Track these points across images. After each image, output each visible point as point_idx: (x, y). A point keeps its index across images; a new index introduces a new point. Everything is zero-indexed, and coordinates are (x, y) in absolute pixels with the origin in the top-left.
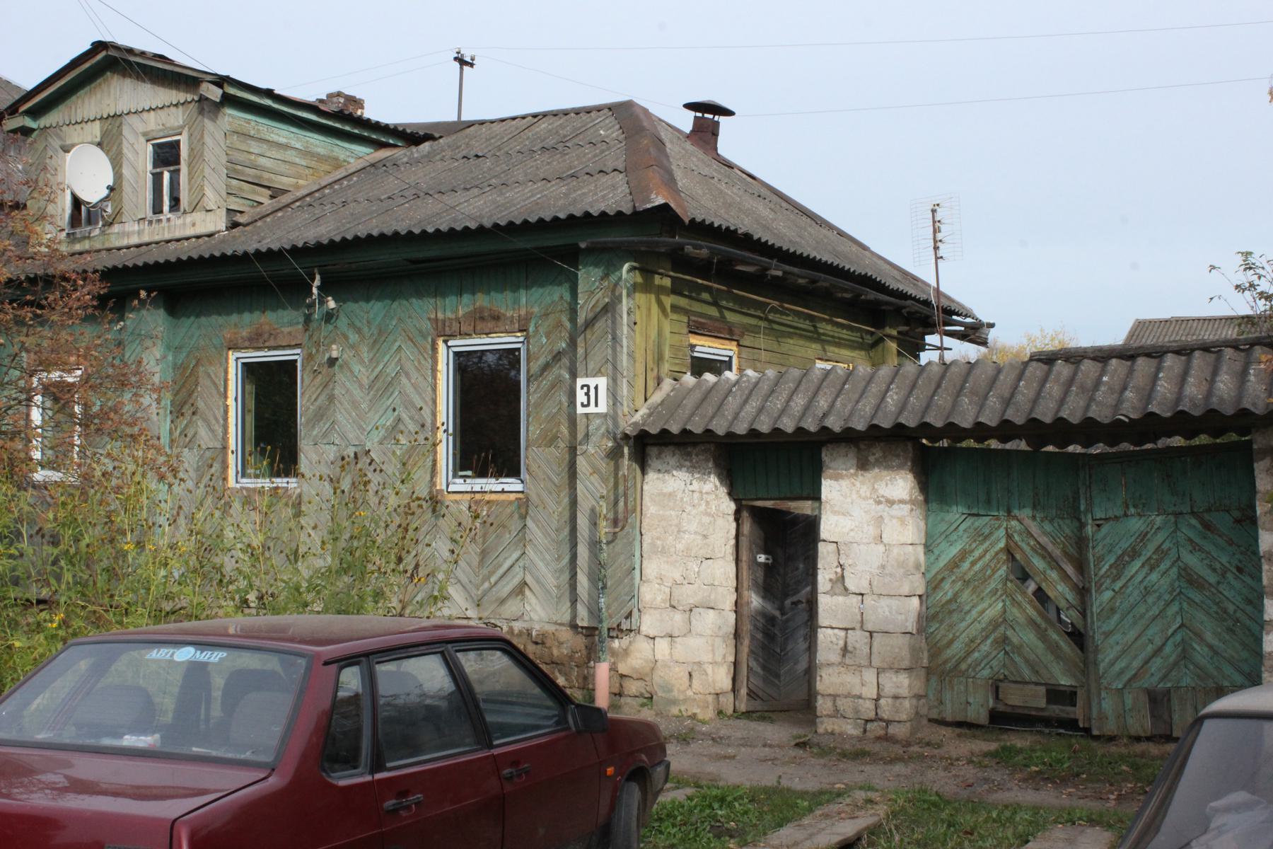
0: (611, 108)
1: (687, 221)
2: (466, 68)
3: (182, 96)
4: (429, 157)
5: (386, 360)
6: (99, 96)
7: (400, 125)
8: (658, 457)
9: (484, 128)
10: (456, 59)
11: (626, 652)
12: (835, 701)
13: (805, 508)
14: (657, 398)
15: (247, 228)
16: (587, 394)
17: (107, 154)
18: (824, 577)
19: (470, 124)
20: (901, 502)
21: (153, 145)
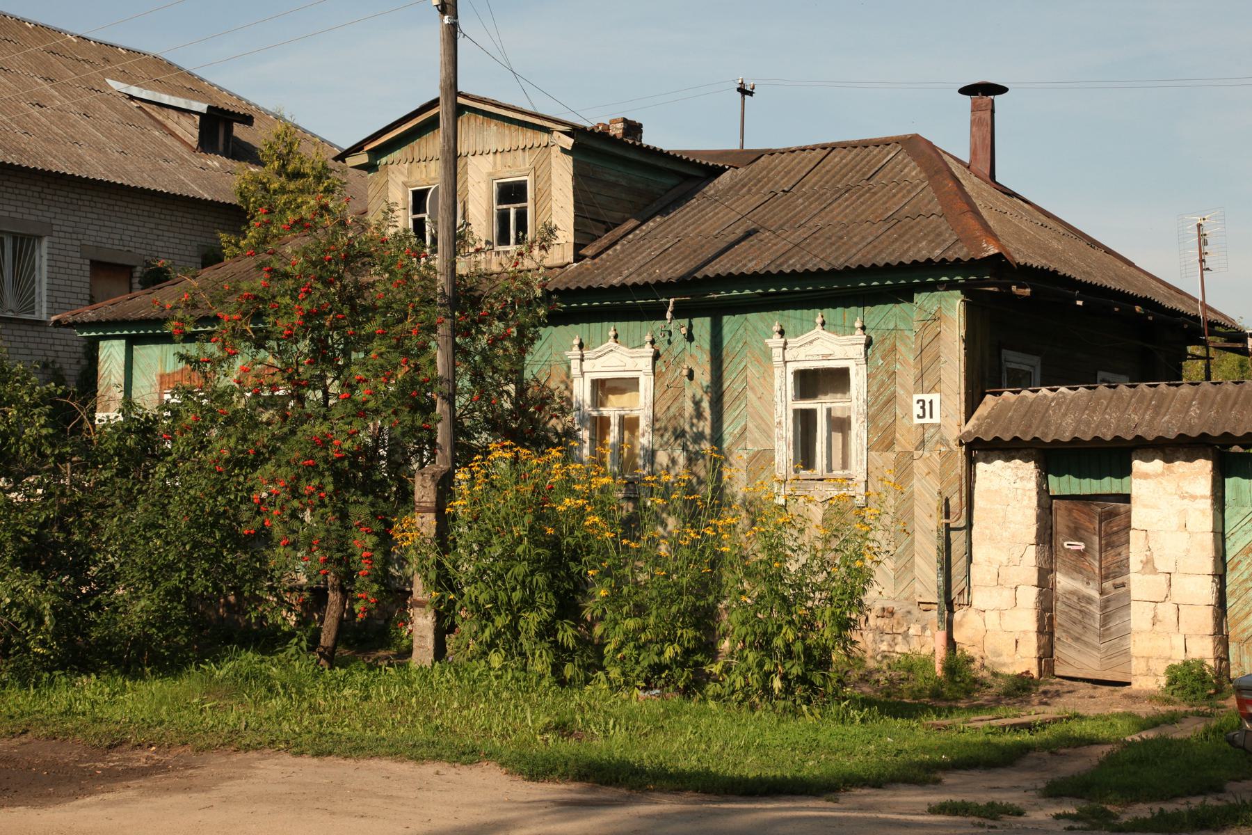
0: (898, 141)
2: (747, 97)
7: (678, 151)
9: (777, 159)
10: (739, 90)
12: (1148, 662)
16: (923, 408)
18: (1135, 563)
19: (759, 155)
20: (1202, 497)
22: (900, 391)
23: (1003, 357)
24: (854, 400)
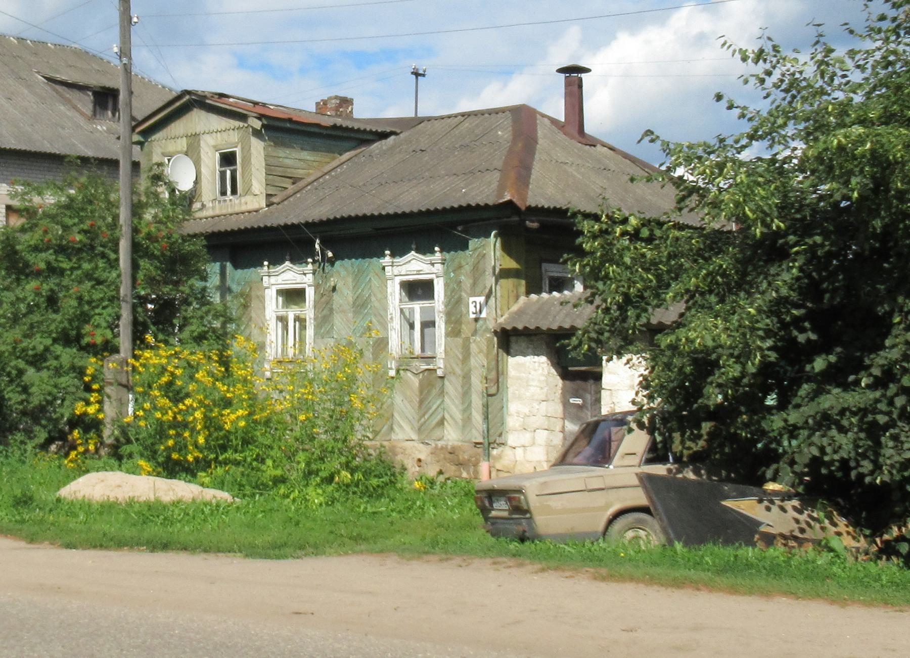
1: (523, 208)
3: (237, 123)
4: (392, 148)
5: (362, 287)
6: (185, 121)
8: (517, 342)
10: (412, 73)
11: (499, 457)
13: (597, 370)
14: (515, 308)
15: (280, 206)
16: (475, 307)
17: (191, 158)
21: (220, 154)
22: (463, 294)
23: (543, 269)
24: (437, 302)
